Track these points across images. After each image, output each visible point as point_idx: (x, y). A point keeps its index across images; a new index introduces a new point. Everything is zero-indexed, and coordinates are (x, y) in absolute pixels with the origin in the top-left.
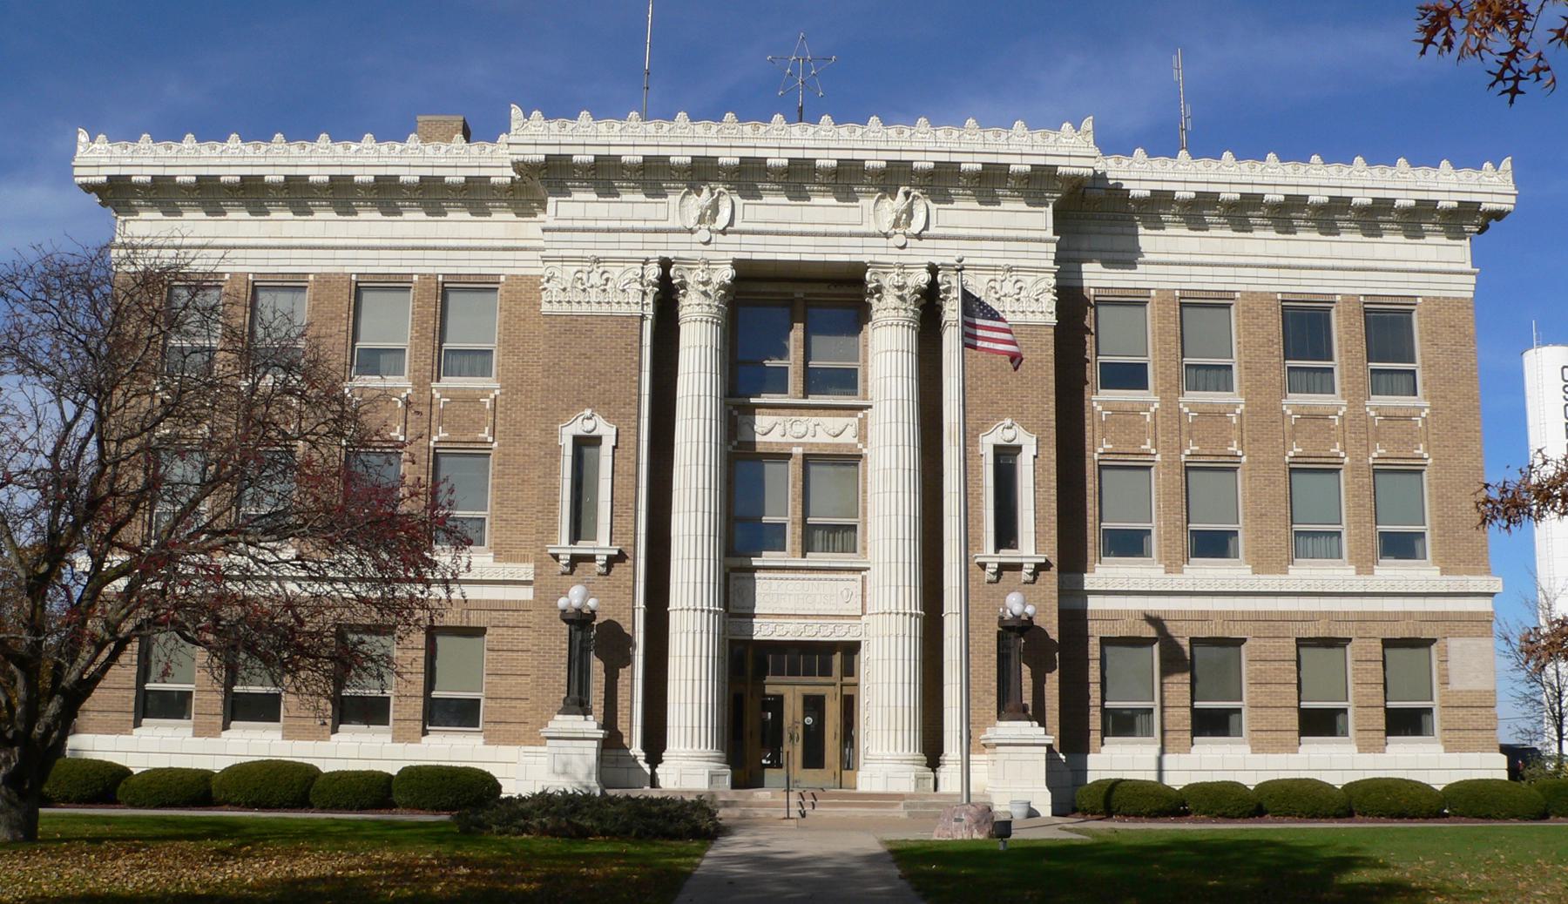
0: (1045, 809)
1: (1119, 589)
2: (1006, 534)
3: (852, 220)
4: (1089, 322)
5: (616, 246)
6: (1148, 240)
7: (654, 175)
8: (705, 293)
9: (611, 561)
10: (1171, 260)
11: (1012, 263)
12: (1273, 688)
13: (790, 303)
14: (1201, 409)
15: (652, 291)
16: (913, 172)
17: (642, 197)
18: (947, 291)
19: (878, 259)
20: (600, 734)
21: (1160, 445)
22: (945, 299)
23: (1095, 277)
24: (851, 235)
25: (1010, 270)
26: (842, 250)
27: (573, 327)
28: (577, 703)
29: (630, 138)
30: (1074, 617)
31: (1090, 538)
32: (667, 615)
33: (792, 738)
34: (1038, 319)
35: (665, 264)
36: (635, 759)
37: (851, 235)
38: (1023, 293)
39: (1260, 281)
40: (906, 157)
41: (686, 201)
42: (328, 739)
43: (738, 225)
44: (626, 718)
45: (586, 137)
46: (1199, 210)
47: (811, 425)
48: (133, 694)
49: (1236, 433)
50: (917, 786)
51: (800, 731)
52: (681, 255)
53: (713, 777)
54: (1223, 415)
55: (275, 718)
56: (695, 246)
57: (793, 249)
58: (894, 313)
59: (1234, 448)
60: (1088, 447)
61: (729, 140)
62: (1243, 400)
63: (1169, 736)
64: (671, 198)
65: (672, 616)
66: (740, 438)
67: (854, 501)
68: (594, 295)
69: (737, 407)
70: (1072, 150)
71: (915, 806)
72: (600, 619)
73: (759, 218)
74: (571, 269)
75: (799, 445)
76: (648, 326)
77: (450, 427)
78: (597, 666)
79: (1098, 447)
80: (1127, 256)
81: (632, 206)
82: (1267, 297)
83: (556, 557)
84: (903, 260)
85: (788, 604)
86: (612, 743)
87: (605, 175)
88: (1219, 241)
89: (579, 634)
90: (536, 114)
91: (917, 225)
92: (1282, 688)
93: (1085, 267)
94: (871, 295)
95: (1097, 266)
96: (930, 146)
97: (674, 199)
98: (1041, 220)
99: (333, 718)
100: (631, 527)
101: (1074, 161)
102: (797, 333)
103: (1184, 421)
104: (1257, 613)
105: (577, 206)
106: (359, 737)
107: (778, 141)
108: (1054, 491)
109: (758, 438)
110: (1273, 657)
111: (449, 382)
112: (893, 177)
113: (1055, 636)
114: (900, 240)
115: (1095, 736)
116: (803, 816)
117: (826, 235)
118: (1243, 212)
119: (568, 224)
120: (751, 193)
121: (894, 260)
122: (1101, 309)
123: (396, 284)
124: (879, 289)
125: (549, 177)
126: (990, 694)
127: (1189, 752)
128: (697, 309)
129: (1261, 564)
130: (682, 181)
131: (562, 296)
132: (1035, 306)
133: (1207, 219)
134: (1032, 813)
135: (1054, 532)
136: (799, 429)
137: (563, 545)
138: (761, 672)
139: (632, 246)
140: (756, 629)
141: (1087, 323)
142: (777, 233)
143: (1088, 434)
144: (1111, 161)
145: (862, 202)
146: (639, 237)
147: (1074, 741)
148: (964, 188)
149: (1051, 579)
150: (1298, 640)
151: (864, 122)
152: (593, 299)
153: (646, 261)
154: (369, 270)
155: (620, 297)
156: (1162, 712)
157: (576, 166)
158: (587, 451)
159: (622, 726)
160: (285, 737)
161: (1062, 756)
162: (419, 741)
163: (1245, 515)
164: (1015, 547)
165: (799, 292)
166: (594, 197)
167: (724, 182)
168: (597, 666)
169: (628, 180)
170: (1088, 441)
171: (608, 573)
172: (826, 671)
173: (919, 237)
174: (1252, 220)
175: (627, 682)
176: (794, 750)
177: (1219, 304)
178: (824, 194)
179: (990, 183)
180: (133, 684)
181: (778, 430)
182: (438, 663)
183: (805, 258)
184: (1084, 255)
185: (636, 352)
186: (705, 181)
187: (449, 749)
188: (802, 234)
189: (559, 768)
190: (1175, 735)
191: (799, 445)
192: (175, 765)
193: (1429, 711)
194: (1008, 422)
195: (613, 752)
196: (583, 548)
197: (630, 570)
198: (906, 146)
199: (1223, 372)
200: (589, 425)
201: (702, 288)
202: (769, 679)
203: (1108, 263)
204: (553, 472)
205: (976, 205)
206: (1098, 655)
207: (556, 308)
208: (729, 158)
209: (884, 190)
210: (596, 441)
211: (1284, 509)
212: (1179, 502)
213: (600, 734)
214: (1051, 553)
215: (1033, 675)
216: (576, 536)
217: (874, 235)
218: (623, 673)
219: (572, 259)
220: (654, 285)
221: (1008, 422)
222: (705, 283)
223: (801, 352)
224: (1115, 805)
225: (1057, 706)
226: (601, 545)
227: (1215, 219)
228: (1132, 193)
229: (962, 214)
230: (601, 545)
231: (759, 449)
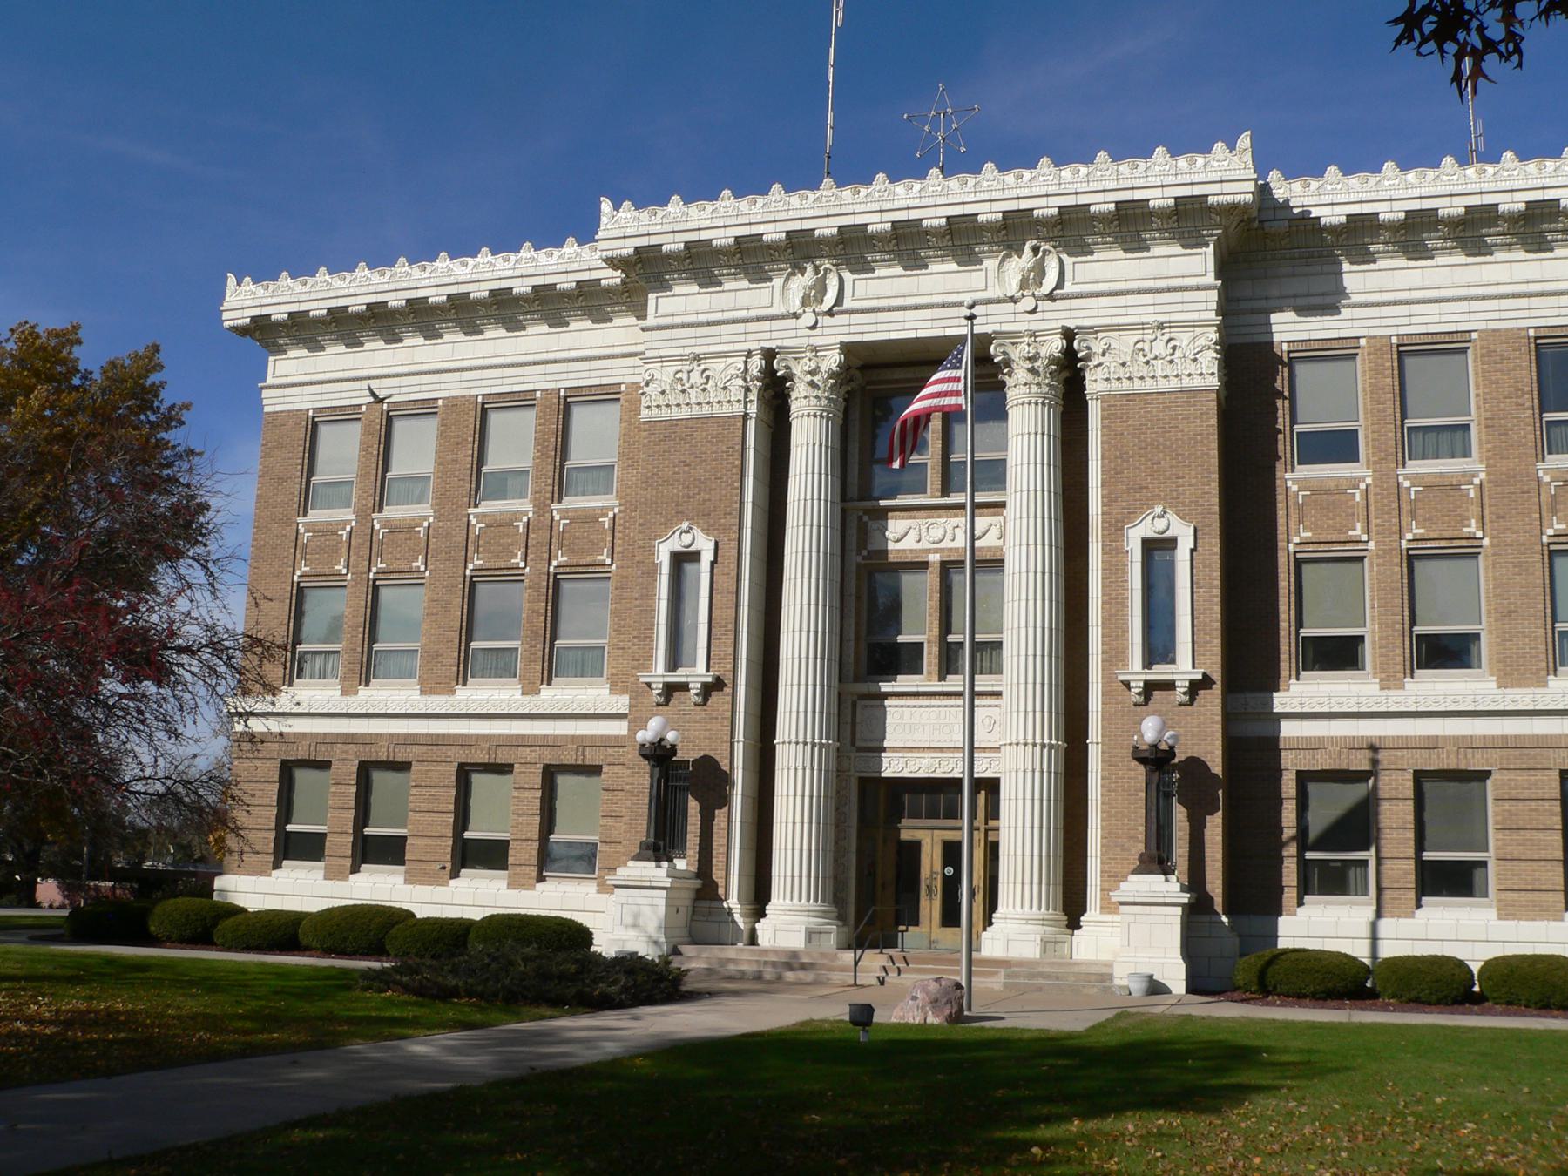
0: (1178, 985)
1: (1316, 712)
2: (1158, 648)
3: (974, 286)
4: (1281, 383)
6: (1354, 278)
7: (751, 258)
9: (708, 690)
10: (1385, 298)
11: (1162, 318)
12: (1528, 834)
14: (1315, 486)
18: (1087, 358)
19: (1005, 328)
20: (1185, 898)
21: (1373, 528)
23: (1287, 328)
25: (1161, 326)
27: (673, 432)
28: (662, 845)
29: (722, 219)
30: (1252, 747)
31: (1284, 648)
32: (774, 747)
33: (930, 890)
34: (1197, 383)
35: (770, 355)
36: (730, 912)
38: (1178, 353)
39: (1504, 315)
41: (1006, 265)
42: (446, 884)
43: (848, 304)
44: (722, 866)
45: (678, 222)
46: (1416, 233)
47: (949, 528)
48: (272, 835)
49: (1475, 509)
50: (1044, 951)
51: (939, 883)
52: (786, 343)
53: (811, 935)
54: (335, 533)
55: (400, 861)
56: (800, 333)
57: (907, 326)
58: (1025, 389)
59: (1472, 528)
60: (1281, 536)
61: (1045, 187)
62: (1482, 467)
63: (1387, 895)
65: (779, 749)
66: (870, 547)
67: (987, 608)
68: (694, 395)
69: (867, 511)
70: (1224, 173)
71: (1016, 975)
72: (1180, 757)
73: (870, 294)
74: (671, 369)
75: (936, 551)
76: (751, 424)
77: (571, 551)
78: (1180, 814)
79: (1294, 537)
80: (1329, 300)
81: (738, 295)
82: (1514, 335)
83: (1127, 684)
84: (1034, 326)
85: (919, 733)
86: (705, 890)
87: (702, 262)
88: (1449, 271)
89: (1155, 777)
90: (627, 204)
92: (1541, 835)
93: (1274, 317)
95: (1290, 316)
97: (991, 264)
98: (1198, 265)
99: (453, 862)
100: (731, 650)
101: (1227, 187)
103: (1404, 497)
104: (1504, 738)
105: (680, 301)
106: (478, 883)
108: (1217, 592)
109: (891, 546)
110: (1526, 794)
111: (1416, 467)
113: (1217, 768)
115: (1290, 895)
116: (882, 983)
117: (943, 306)
118: (1474, 230)
119: (668, 321)
120: (862, 266)
122: (1300, 369)
123: (517, 401)
125: (647, 270)
126: (1134, 838)
127: (1412, 916)
129: (1509, 676)
131: (1121, 372)
132: (1192, 368)
133: (1430, 244)
134: (1155, 988)
135: (1218, 642)
136: (936, 533)
137: (658, 673)
138: (896, 814)
140: (885, 764)
141: (1278, 385)
142: (889, 309)
143: (1281, 521)
144: (1296, 186)
146: (740, 327)
147: (1255, 895)
148: (1102, 234)
149: (1212, 700)
150: (1416, 773)
152: (694, 400)
153: (749, 354)
154: (494, 390)
156: (1379, 864)
157: (927, 232)
158: (1158, 555)
159: (717, 874)
160: (407, 881)
161: (1224, 919)
162: (532, 888)
163: (1489, 612)
164: (1173, 661)
166: (695, 288)
167: (830, 257)
168: (1180, 814)
169: (728, 266)
170: (1281, 529)
171: (705, 703)
172: (953, 813)
174: (1489, 240)
175: (724, 825)
176: (931, 907)
177: (1452, 347)
178: (942, 259)
179: (1130, 224)
180: (273, 825)
181: (913, 535)
182: (558, 804)
183: (922, 334)
184: (1272, 303)
185: (738, 455)
187: (378, 887)
189: (628, 919)
190: (1395, 894)
191: (936, 551)
192: (1326, 948)
193: (1483, 864)
194: (1159, 509)
195: (706, 904)
196: (1160, 672)
197: (729, 699)
198: (1083, 187)
199: (1459, 434)
200: (1161, 524)
201: (809, 378)
202: (905, 822)
203: (1303, 310)
204: (649, 594)
205: (1120, 254)
206: (1293, 793)
207: (656, 414)
210: (695, 556)
211: (1540, 603)
212: (1398, 600)
213: (1185, 898)
214: (1213, 665)
215: (1191, 818)
216: (673, 663)
217: (999, 301)
218: (720, 814)
219: (1131, 327)
221: (1159, 509)
224: (1270, 982)
225: (1219, 856)
226: (1183, 669)
227: (1439, 244)
228: (1323, 221)
229: (1106, 266)
230: (697, 673)
231: (892, 558)
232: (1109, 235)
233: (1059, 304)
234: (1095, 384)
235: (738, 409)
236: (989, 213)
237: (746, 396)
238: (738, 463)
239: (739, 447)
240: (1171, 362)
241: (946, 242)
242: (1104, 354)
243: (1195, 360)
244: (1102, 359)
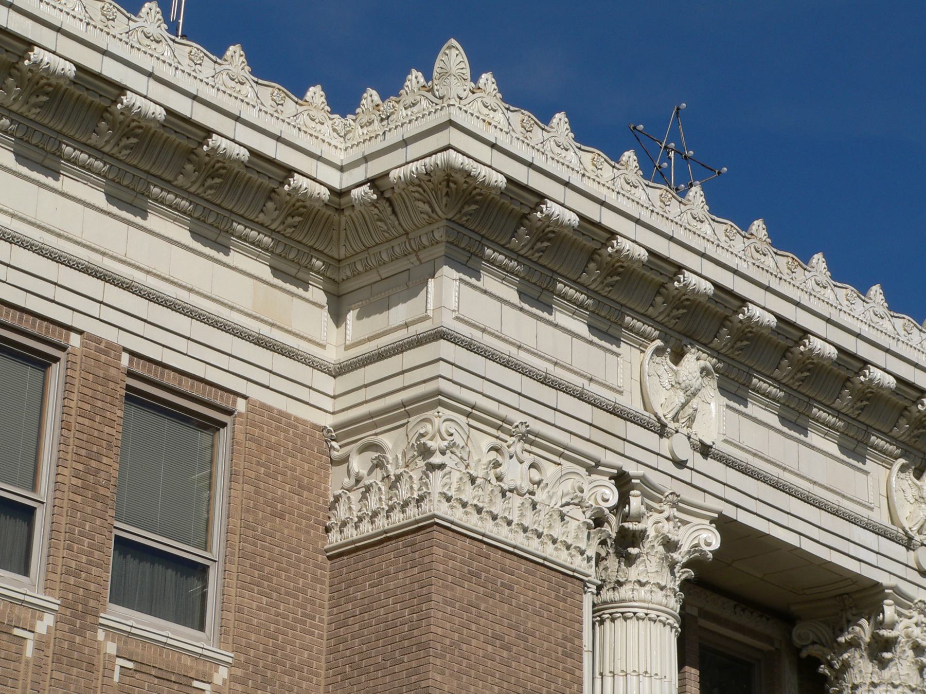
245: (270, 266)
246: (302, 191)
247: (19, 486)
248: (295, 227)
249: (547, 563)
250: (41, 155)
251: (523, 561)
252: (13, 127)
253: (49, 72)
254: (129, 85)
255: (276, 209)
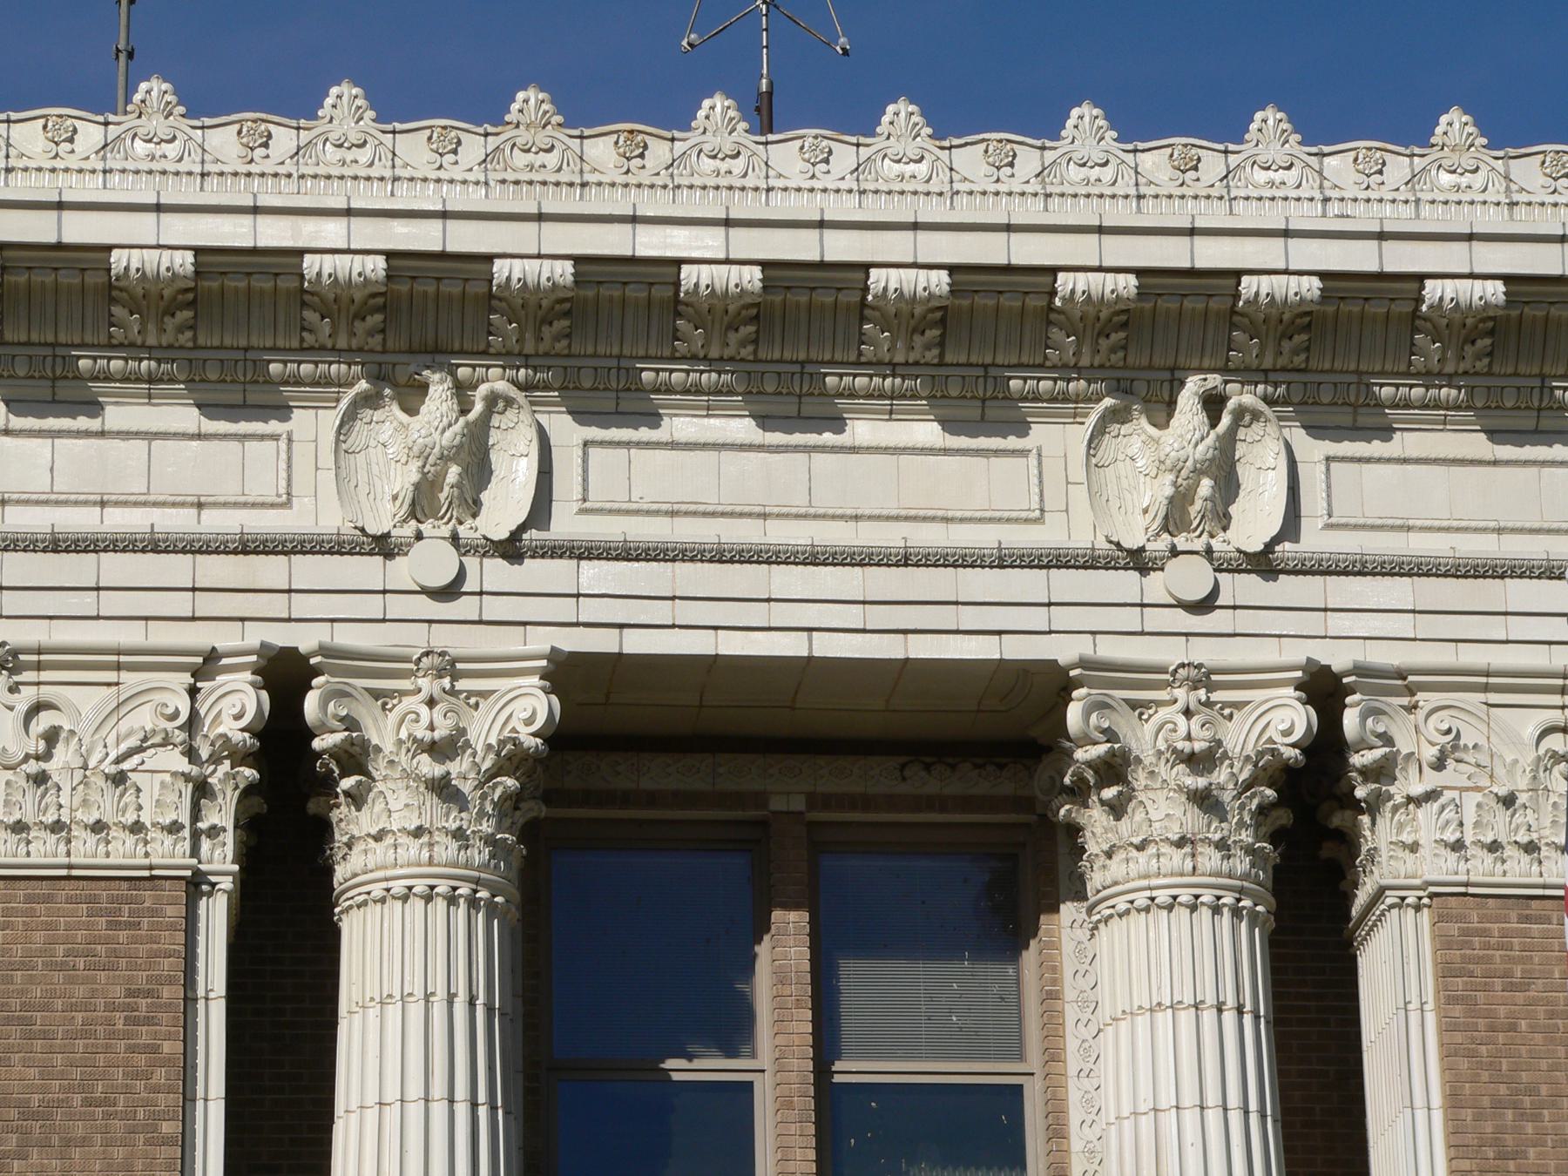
5: (84, 603)
8: (443, 789)
13: (753, 837)
15: (230, 783)
16: (492, 300)
17: (186, 417)
18: (1382, 772)
19: (1110, 650)
22: (1373, 807)
24: (1003, 561)
26: (970, 618)
35: (285, 675)
37: (1003, 561)
38: (64, 755)
40: (1212, 254)
43: (565, 524)
56: (399, 606)
58: (1177, 859)
61: (529, 192)
64: (301, 420)
76: (215, 916)
84: (1206, 653)
91: (1255, 520)
94: (1079, 792)
96: (1304, 216)
97: (313, 425)
102: (782, 953)
107: (717, 198)
112: (1161, 336)
114: (1192, 578)
117: (905, 560)
120: (615, 400)
121: (1170, 653)
124: (1115, 769)
128: (413, 849)
130: (1089, 373)
131: (1500, 826)
139: (145, 604)
142: (721, 556)
145: (1040, 434)
146: (177, 568)
148: (1429, 377)
151: (1047, 126)
153: (208, 664)
155: (105, 804)
165: (787, 791)
167: (509, 357)
169: (131, 348)
173: (1263, 564)
178: (892, 404)
185: (168, 1021)
186: (438, 353)
188: (814, 558)
201: (428, 767)
205: (1477, 444)
208: (533, 259)
209: (1122, 388)
220: (240, 757)
222: (442, 749)
223: (802, 1023)
232: (1450, 380)
233: (1288, 589)
234: (1401, 851)
235: (169, 853)
236: (343, 252)
237: (196, 815)
238: (172, 1047)
239: (172, 993)
240: (40, 779)
241: (922, 349)
242: (1439, 765)
243: (119, 779)
244: (1432, 780)
245: (570, 413)
246: (1448, 305)
247: (919, 1058)
248: (383, 331)
249: (75, 873)
250: (55, 390)
251: (18, 884)
252: (1281, 390)
253: (907, 301)
254: (300, 244)
255: (323, 318)
